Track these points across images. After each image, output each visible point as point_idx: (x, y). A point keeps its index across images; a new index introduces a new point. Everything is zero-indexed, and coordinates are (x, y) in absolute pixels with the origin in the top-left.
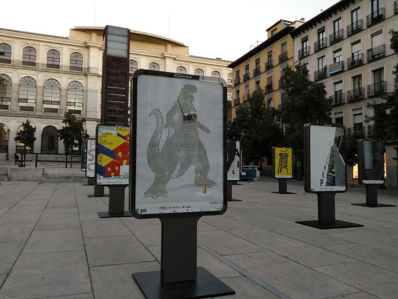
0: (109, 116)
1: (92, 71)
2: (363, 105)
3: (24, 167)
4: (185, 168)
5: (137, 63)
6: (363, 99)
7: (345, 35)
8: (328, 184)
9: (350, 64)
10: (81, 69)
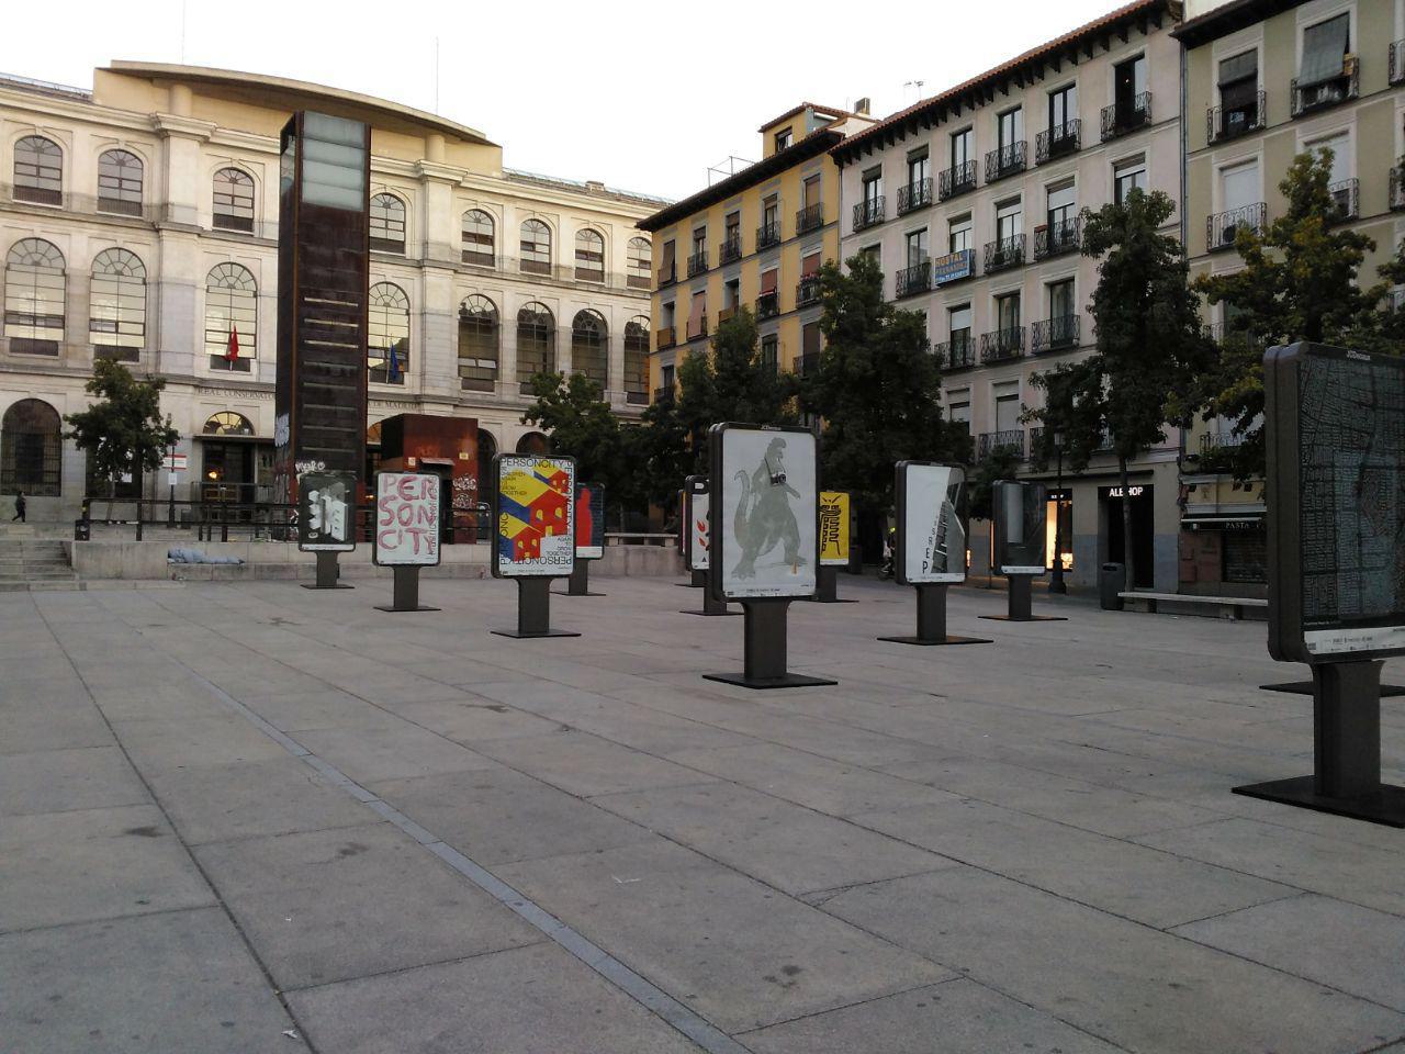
0: (309, 388)
1: (178, 216)
2: (1020, 373)
3: (87, 539)
4: (773, 543)
6: (1020, 358)
7: (981, 179)
8: (936, 569)
9: (991, 261)
10: (137, 207)
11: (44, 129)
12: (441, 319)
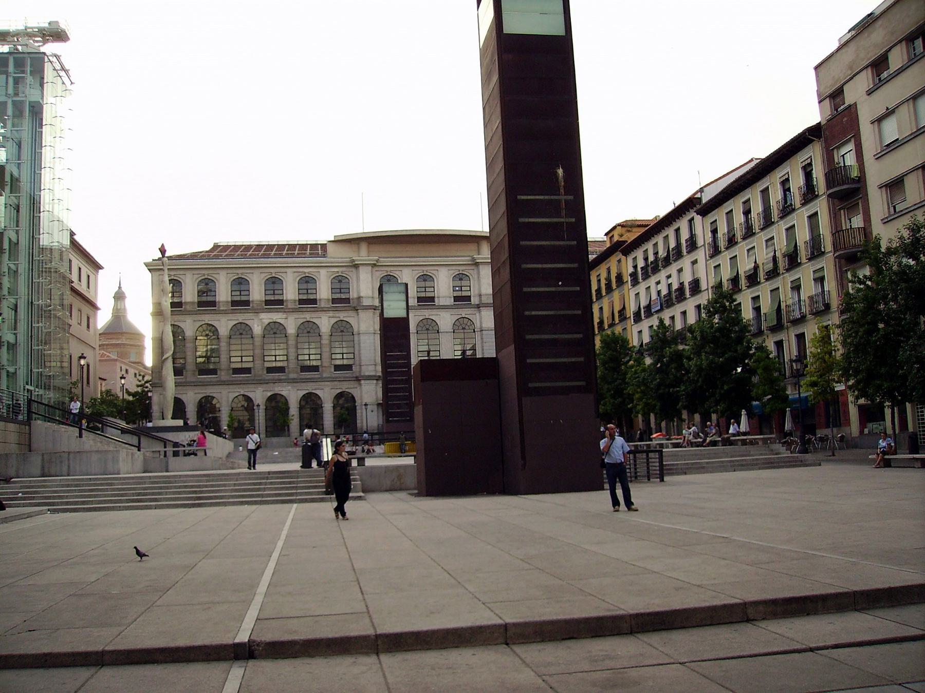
10: (347, 300)
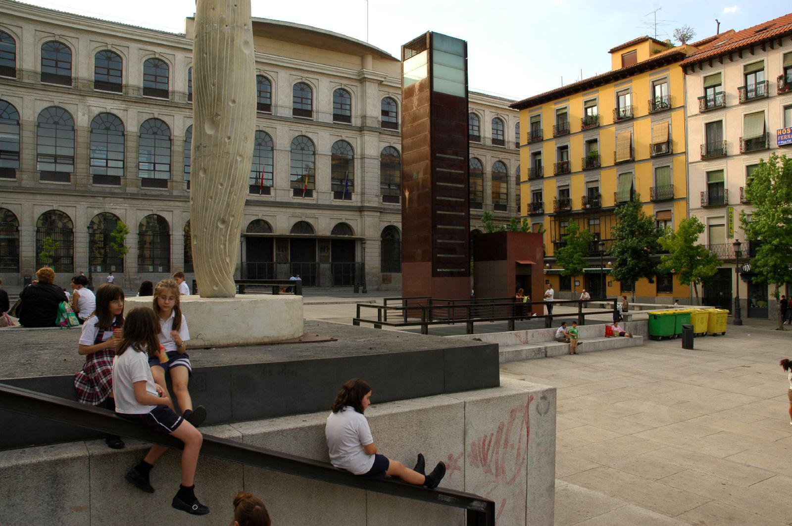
5: (15, 41)
11: (160, 54)
12: (372, 161)
